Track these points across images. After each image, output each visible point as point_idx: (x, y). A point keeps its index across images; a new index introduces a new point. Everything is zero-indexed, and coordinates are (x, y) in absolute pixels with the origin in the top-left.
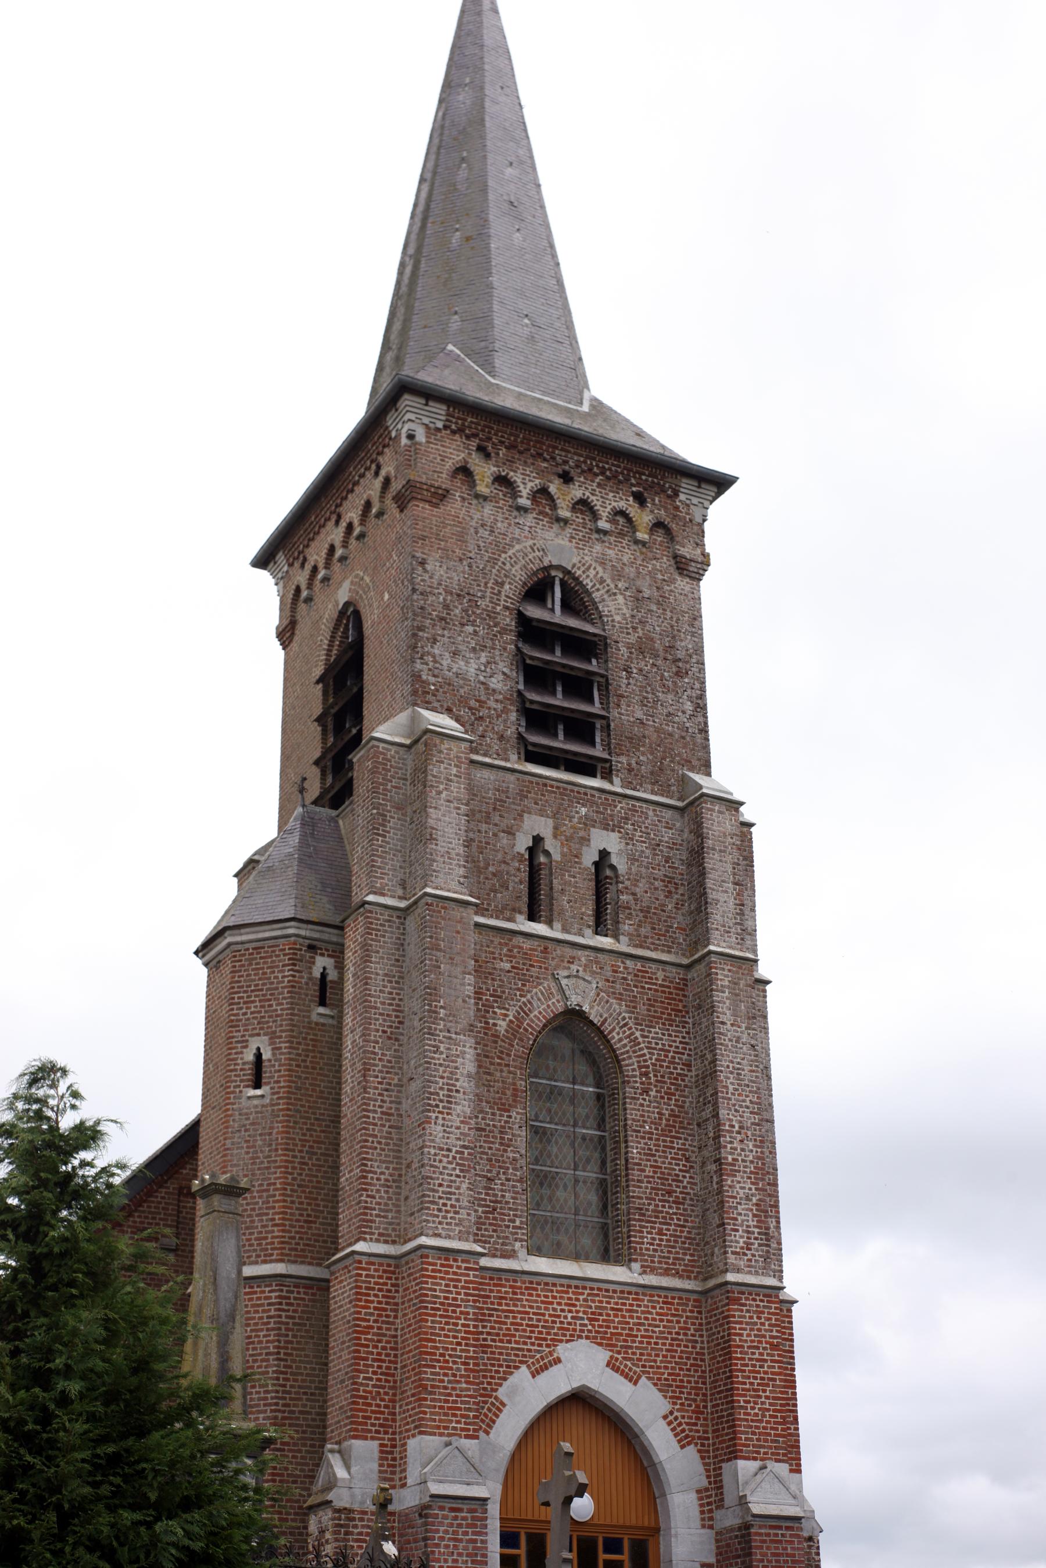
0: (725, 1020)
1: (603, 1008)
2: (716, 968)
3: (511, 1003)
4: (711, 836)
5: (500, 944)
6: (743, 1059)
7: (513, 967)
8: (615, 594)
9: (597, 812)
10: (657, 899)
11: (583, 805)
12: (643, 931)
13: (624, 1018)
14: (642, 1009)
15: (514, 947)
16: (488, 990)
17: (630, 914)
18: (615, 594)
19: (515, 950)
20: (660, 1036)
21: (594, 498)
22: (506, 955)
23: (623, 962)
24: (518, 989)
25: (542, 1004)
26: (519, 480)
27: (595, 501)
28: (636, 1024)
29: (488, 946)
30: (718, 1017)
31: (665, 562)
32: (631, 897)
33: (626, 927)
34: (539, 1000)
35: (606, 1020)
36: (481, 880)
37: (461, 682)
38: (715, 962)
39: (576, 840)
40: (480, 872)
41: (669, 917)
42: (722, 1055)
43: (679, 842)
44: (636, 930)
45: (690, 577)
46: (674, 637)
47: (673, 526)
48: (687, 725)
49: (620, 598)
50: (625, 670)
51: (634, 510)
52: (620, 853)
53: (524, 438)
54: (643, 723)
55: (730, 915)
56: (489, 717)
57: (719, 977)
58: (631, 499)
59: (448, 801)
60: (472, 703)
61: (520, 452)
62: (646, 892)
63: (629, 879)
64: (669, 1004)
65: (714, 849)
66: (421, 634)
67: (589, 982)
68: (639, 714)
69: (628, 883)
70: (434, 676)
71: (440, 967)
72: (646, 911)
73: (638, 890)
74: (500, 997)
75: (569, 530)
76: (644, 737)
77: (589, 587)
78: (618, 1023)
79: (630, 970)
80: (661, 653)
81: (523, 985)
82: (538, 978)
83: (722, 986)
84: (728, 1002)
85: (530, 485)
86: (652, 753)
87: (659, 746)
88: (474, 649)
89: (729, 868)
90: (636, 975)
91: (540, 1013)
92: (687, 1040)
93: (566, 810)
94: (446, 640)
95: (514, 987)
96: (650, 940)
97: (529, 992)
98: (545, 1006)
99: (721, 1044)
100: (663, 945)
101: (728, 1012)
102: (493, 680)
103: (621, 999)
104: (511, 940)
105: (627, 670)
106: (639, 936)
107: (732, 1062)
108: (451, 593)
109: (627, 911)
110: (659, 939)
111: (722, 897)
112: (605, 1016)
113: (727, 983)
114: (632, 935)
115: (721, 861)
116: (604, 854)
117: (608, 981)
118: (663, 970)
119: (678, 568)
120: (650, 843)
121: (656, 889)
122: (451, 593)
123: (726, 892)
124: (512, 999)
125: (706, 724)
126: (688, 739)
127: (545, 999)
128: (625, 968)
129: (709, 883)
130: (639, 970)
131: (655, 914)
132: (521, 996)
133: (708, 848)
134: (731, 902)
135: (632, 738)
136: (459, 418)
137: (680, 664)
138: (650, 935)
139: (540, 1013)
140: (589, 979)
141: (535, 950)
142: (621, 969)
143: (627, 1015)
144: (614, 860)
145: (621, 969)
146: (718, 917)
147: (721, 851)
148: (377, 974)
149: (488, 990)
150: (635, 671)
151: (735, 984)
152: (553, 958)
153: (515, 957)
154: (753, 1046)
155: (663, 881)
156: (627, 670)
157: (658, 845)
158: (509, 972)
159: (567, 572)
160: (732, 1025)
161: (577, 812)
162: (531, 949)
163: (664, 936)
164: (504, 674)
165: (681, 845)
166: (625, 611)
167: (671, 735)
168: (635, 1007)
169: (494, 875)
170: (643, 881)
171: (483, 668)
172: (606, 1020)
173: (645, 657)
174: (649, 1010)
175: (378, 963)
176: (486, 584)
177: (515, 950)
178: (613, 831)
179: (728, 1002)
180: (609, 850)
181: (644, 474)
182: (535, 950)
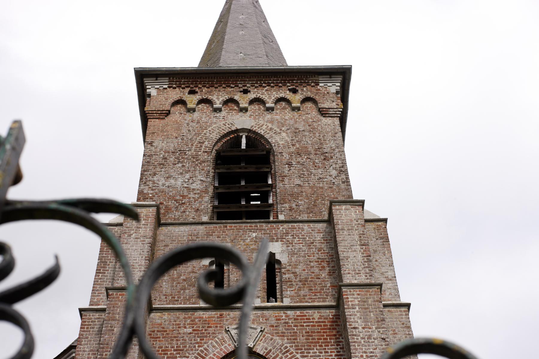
0: (357, 326)
1: (267, 343)
2: (346, 295)
3: (191, 352)
4: (340, 223)
5: (185, 318)
6: (375, 349)
7: (193, 330)
8: (280, 133)
9: (264, 234)
10: (313, 273)
11: (254, 232)
12: (302, 293)
13: (286, 347)
14: (301, 339)
15: (196, 318)
16: (173, 347)
17: (292, 284)
18: (280, 133)
19: (197, 320)
20: (318, 354)
21: (263, 96)
22: (189, 324)
23: (284, 313)
24: (197, 343)
25: (217, 349)
26: (214, 99)
27: (265, 97)
28: (296, 350)
29: (175, 321)
30: (350, 325)
31: (315, 113)
32: (292, 275)
33: (289, 293)
34: (214, 346)
35: (270, 351)
36: (174, 285)
37: (171, 189)
38: (346, 292)
39: (249, 251)
40: (174, 281)
41: (323, 281)
42: (356, 349)
43: (329, 238)
44: (296, 293)
45: (331, 117)
46: (321, 144)
47: (317, 98)
48: (334, 181)
49: (284, 134)
50: (287, 164)
51: (289, 95)
52: (282, 252)
53: (217, 81)
54: (301, 186)
55: (359, 264)
56: (189, 202)
57: (350, 300)
58: (288, 92)
59: (136, 238)
60: (178, 198)
61: (215, 88)
62: (304, 270)
63: (290, 265)
64: (324, 332)
65: (342, 229)
66: (146, 173)
67: (255, 329)
68: (298, 182)
69: (288, 268)
70: (152, 190)
71: (113, 330)
72: (304, 282)
73: (297, 270)
74: (182, 350)
75: (248, 113)
76: (302, 192)
77: (262, 133)
78: (281, 352)
79: (291, 317)
80: (313, 152)
81: (201, 340)
82: (213, 333)
83: (352, 305)
84: (358, 314)
85: (221, 99)
86: (308, 199)
87: (313, 194)
88: (181, 174)
89: (357, 238)
90: (295, 319)
91: (214, 355)
92: (341, 353)
93: (241, 237)
94: (162, 173)
95: (193, 342)
96: (308, 297)
97: (205, 343)
98: (219, 350)
99: (355, 342)
100: (319, 298)
101: (359, 321)
102: (193, 185)
103: (283, 336)
104: (193, 315)
105: (290, 164)
106: (299, 296)
107: (365, 352)
108: (169, 152)
109: (289, 283)
110: (315, 295)
111: (351, 255)
112: (269, 348)
113: (357, 303)
114: (293, 296)
115: (349, 235)
116: (272, 255)
117: (273, 326)
118: (318, 312)
119: (322, 114)
120: (306, 243)
121: (312, 267)
122: (169, 152)
123: (355, 251)
124: (192, 350)
125: (347, 178)
126: (334, 187)
127: (219, 345)
128: (286, 316)
129: (340, 249)
130: (297, 316)
131: (311, 281)
132: (199, 347)
133: (339, 229)
134: (360, 257)
135: (293, 194)
136: (176, 82)
137: (327, 155)
138: (308, 294)
139: (214, 355)
140: (255, 327)
141: (213, 317)
142: (284, 317)
143: (288, 345)
144: (278, 257)
145: (284, 317)
146: (350, 266)
147: (349, 230)
148: (84, 351)
149: (173, 347)
150: (294, 163)
151: (364, 302)
152: (227, 320)
153: (196, 324)
154: (383, 339)
155: (318, 262)
156: (290, 164)
157: (313, 243)
158: (190, 333)
159: (249, 131)
160: (363, 328)
161: (249, 236)
162: (209, 318)
163: (320, 292)
164: (201, 180)
165: (330, 240)
166: (287, 138)
167: (322, 188)
168: (296, 339)
169: (184, 280)
170: (301, 264)
171: (187, 181)
172: (270, 351)
173: (301, 156)
174: (307, 339)
175: (87, 344)
176: (192, 145)
177: (197, 320)
178: (277, 241)
179: (358, 314)
180: (274, 252)
181: (295, 80)
182: (213, 317)
